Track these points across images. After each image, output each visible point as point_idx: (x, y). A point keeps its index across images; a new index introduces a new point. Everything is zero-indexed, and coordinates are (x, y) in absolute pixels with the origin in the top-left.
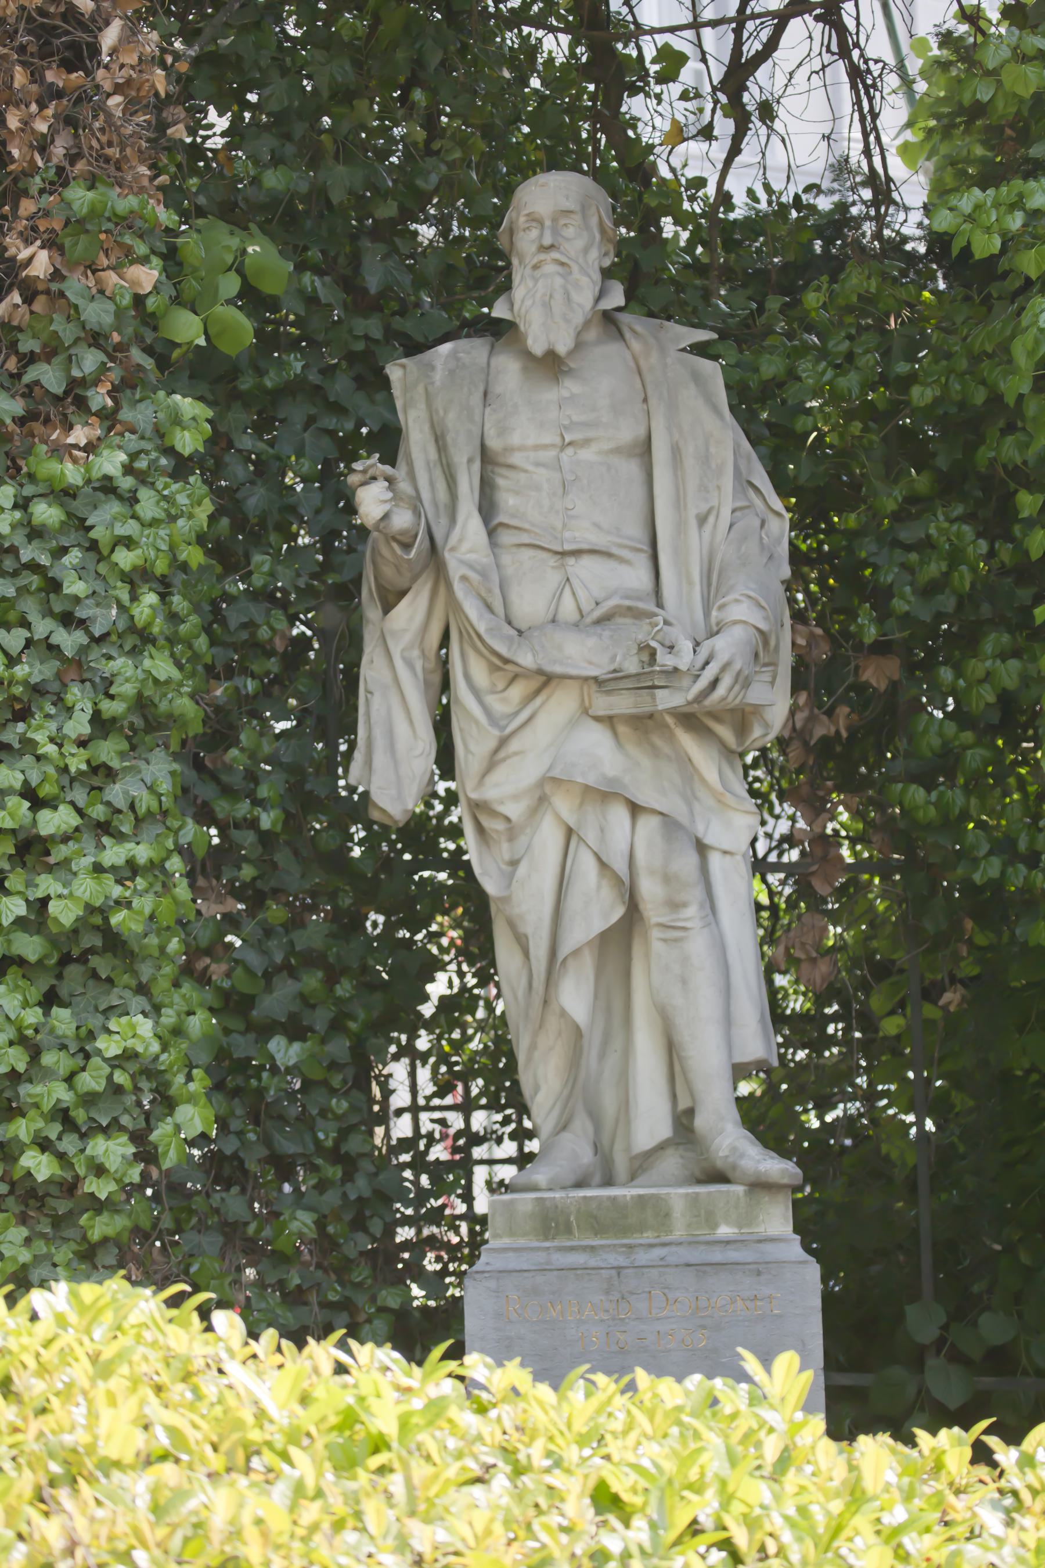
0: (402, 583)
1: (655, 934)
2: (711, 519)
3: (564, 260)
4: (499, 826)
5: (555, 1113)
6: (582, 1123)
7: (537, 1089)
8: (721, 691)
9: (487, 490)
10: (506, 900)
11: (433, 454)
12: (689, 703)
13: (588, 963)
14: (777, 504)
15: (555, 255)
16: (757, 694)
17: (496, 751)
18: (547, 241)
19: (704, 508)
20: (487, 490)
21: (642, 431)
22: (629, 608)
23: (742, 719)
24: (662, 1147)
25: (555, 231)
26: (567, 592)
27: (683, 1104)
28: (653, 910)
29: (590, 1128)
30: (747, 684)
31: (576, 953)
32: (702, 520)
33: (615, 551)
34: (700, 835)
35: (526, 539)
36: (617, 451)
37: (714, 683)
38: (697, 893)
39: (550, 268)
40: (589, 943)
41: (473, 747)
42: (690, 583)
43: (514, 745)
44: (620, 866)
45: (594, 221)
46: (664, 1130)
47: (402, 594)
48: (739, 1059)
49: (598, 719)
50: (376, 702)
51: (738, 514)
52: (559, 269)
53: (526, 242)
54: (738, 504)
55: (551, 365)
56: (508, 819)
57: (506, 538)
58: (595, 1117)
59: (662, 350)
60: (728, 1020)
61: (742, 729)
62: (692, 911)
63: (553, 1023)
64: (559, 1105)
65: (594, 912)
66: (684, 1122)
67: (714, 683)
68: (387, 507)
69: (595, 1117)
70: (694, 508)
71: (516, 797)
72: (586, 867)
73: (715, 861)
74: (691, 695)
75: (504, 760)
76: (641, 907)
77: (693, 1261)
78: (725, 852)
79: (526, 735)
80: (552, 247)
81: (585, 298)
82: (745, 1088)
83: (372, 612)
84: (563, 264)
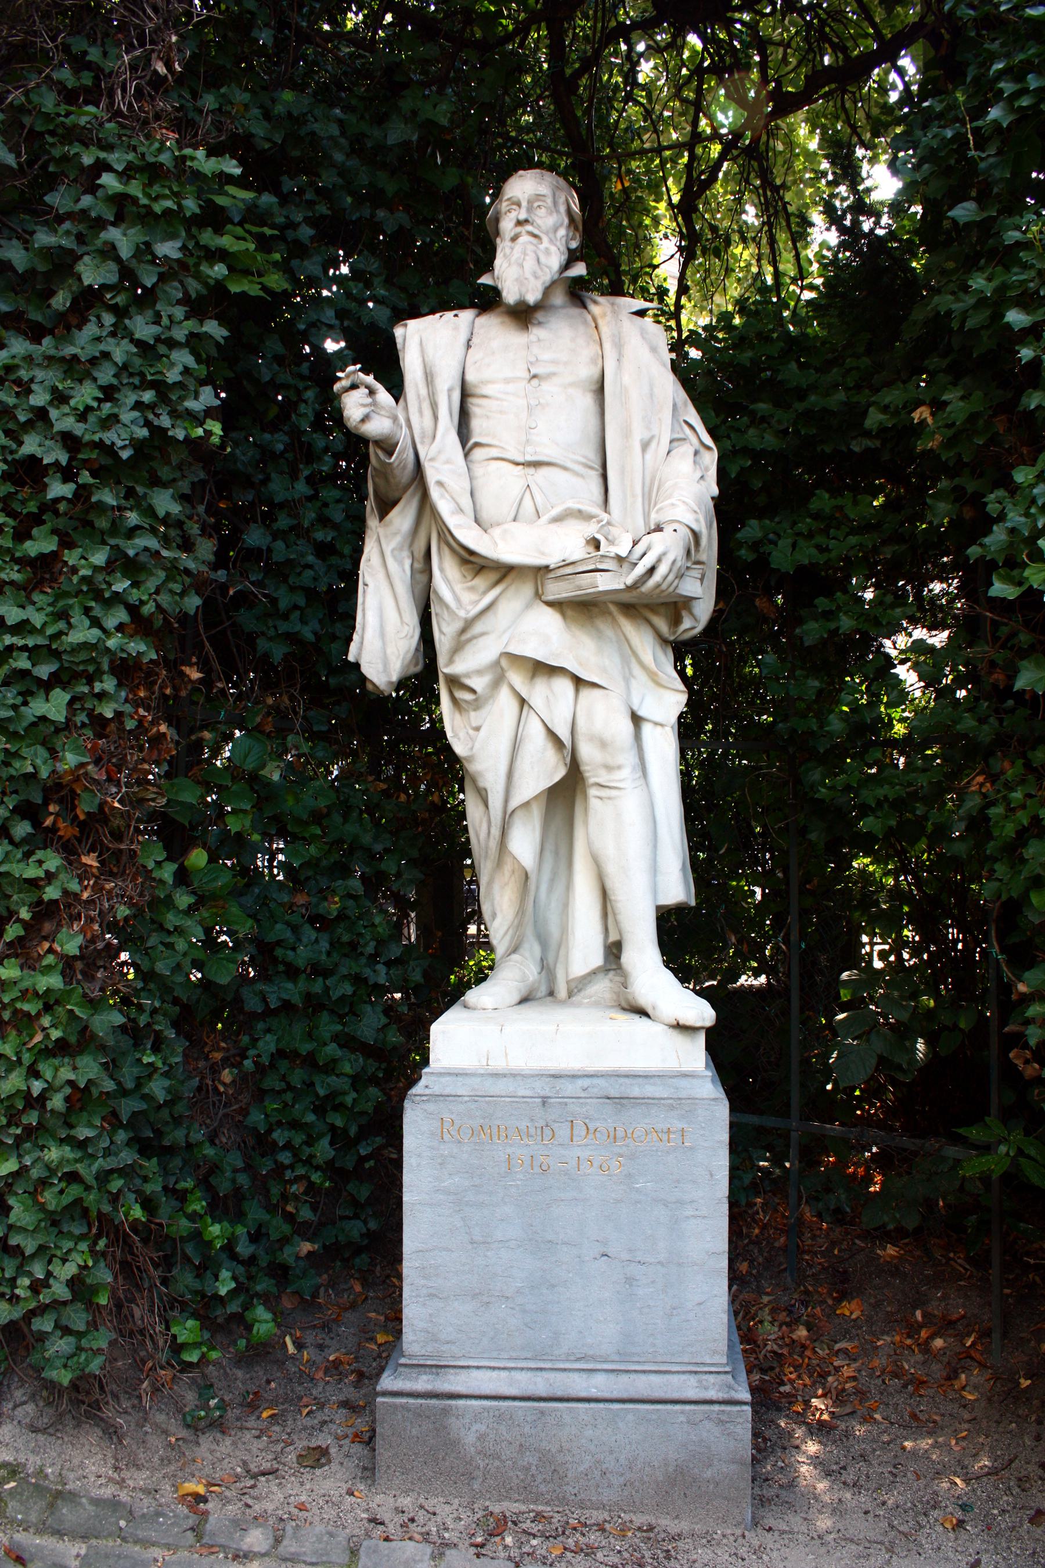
0: (397, 495)
1: (593, 792)
2: (653, 445)
3: (536, 232)
4: (467, 696)
5: (508, 937)
6: (532, 949)
7: (494, 916)
8: (657, 577)
9: (464, 418)
10: (470, 759)
11: (424, 392)
12: (629, 588)
13: (537, 813)
14: (708, 440)
15: (529, 228)
16: (691, 587)
17: (463, 631)
18: (523, 216)
19: (646, 436)
20: (464, 418)
21: (595, 372)
22: (580, 511)
23: (676, 607)
24: (594, 973)
25: (530, 210)
26: (528, 495)
27: (613, 938)
28: (593, 774)
29: (537, 950)
30: (680, 576)
31: (527, 805)
32: (645, 446)
33: (569, 465)
34: (635, 708)
35: (494, 452)
36: (571, 385)
37: (652, 570)
38: (628, 759)
39: (524, 239)
40: (536, 798)
41: (444, 630)
42: (634, 496)
43: (478, 628)
44: (564, 735)
45: (563, 209)
46: (597, 959)
47: (395, 503)
48: (571, 976)
49: (550, 604)
50: (370, 590)
51: (675, 444)
52: (532, 239)
53: (507, 225)
54: (676, 436)
55: (524, 315)
56: (474, 691)
57: (478, 454)
58: (543, 941)
59: (615, 312)
60: (654, 869)
61: (676, 621)
62: (626, 773)
63: (507, 868)
64: (510, 932)
65: (540, 771)
66: (614, 951)
67: (652, 570)
68: (366, 410)
69: (543, 941)
70: (638, 435)
71: (479, 672)
72: (534, 731)
73: (647, 729)
74: (630, 580)
75: (470, 640)
76: (583, 768)
77: (613, 1093)
78: (656, 724)
79: (489, 617)
80: (526, 221)
81: (555, 260)
82: (469, 862)
83: (372, 522)
84: (535, 236)
